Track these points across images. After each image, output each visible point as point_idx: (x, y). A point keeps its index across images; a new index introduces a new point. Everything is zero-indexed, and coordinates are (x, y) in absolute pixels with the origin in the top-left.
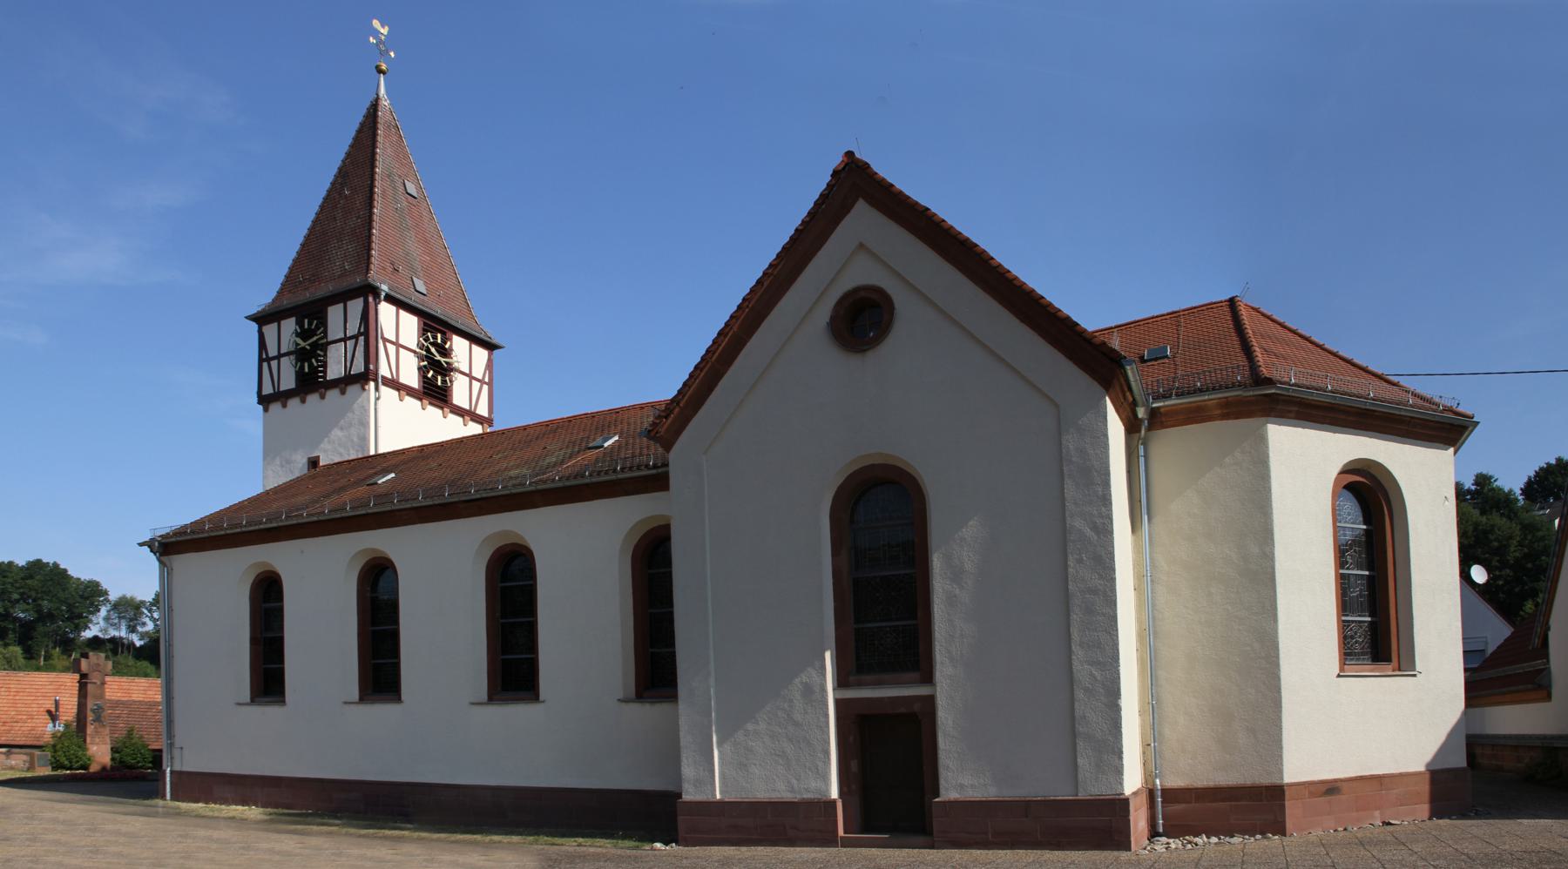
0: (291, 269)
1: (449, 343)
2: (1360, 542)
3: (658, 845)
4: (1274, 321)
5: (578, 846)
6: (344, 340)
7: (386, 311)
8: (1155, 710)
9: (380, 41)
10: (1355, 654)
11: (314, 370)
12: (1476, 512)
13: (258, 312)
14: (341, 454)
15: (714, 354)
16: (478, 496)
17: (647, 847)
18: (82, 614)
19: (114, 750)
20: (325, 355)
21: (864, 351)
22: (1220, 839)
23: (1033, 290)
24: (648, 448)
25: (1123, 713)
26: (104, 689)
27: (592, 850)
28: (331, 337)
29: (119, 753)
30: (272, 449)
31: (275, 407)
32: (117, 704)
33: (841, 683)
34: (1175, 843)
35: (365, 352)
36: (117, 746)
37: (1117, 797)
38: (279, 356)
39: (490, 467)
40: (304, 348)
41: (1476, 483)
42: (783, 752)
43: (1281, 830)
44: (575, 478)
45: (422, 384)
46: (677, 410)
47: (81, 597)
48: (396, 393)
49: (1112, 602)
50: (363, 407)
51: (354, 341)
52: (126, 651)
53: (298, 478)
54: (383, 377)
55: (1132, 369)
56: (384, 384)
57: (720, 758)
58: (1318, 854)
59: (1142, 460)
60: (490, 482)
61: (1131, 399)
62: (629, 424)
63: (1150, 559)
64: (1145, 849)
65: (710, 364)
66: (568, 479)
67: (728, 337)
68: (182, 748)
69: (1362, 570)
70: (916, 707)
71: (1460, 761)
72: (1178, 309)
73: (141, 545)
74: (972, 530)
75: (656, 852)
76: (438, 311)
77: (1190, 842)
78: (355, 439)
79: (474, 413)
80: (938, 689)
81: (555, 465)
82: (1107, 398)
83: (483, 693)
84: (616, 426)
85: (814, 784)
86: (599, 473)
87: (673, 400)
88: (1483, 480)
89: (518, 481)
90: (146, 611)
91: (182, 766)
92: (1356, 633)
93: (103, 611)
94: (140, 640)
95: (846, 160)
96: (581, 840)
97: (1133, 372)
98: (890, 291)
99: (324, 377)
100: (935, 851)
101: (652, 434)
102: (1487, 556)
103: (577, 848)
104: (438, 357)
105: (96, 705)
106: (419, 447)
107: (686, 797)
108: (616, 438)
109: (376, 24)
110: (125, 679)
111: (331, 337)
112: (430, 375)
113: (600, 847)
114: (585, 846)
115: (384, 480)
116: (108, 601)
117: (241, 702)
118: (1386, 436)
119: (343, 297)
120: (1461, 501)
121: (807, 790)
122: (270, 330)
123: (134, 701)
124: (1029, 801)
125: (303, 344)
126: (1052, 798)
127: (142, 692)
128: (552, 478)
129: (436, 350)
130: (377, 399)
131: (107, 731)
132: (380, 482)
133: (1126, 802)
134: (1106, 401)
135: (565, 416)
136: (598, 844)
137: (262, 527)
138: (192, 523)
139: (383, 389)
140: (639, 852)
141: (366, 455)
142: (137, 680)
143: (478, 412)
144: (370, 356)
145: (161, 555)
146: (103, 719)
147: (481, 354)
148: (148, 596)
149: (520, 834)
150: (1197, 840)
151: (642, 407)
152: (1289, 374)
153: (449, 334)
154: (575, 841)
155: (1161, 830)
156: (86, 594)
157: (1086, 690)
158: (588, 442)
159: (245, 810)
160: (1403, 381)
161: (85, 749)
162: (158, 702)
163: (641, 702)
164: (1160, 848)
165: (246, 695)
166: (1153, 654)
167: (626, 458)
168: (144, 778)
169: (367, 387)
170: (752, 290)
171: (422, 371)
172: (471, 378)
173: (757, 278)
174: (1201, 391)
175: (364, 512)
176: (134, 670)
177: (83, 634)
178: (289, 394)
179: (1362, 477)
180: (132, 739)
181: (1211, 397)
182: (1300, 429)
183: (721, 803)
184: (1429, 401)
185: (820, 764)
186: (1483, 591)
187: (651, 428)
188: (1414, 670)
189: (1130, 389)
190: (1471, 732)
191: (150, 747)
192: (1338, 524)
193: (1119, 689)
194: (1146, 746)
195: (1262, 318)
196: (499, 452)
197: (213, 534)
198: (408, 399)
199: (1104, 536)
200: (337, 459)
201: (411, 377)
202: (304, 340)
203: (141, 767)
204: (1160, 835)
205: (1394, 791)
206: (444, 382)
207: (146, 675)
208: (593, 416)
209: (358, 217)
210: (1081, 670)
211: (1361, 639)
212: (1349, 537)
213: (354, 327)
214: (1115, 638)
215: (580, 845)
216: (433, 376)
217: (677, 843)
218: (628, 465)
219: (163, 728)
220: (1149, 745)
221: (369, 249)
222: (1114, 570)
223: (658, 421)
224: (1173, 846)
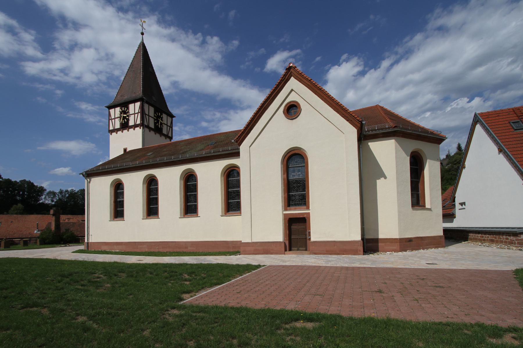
38: (115, 119)
51: (137, 114)
70: (305, 216)
76: (122, 101)
98: (299, 102)
122: (112, 111)
143: (169, 135)
205: (426, 241)
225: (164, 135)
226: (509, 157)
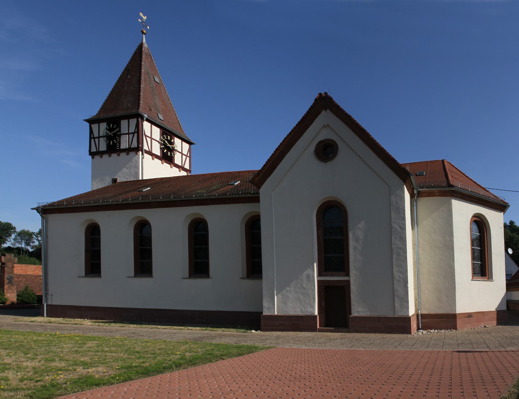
0: (104, 104)
1: (173, 140)
2: (478, 238)
3: (253, 331)
4: (454, 167)
5: (223, 331)
6: (129, 134)
7: (146, 125)
8: (419, 288)
9: (143, 22)
10: (476, 274)
11: (115, 145)
12: (510, 232)
13: (89, 119)
14: (127, 178)
15: (274, 156)
16: (185, 199)
17: (249, 332)
18: (2, 236)
19: (18, 296)
20: (120, 139)
21: (327, 162)
22: (438, 331)
23: (383, 148)
24: (251, 186)
25: (409, 289)
26: (13, 269)
27: (228, 333)
28: (122, 132)
29: (21, 297)
30: (94, 176)
31: (97, 158)
32: (20, 276)
33: (320, 274)
34: (425, 332)
35: (137, 140)
36: (20, 294)
37: (407, 316)
38: (99, 137)
39: (190, 188)
40: (110, 135)
41: (510, 223)
42: (299, 298)
43: (456, 328)
44: (224, 195)
45: (162, 154)
46: (261, 174)
47: (2, 229)
48: (151, 157)
49: (405, 252)
50: (137, 161)
51: (132, 135)
52: (24, 254)
53: (107, 186)
54: (145, 150)
55: (413, 177)
56: (145, 153)
57: (277, 300)
58: (466, 336)
59: (415, 207)
60: (190, 194)
61: (412, 187)
62: (244, 177)
63: (417, 239)
64: (416, 334)
65: (273, 159)
66: (221, 195)
67: (279, 151)
68: (52, 295)
69: (478, 247)
71: (504, 308)
72: (428, 161)
73: (32, 209)
74: (362, 225)
75: (253, 334)
76: (169, 127)
77: (429, 332)
78: (133, 173)
79: (184, 167)
80: (351, 278)
81: (216, 190)
82: (405, 186)
83: (187, 274)
84: (239, 178)
85: (310, 310)
86: (233, 194)
87: (260, 171)
88: (512, 223)
89: (201, 195)
90: (34, 237)
91: (52, 302)
92: (477, 267)
93: (13, 236)
94: (32, 249)
95: (319, 96)
96: (224, 329)
97: (413, 178)
99: (120, 147)
100: (350, 334)
101: (253, 182)
102: (513, 245)
103: (223, 332)
104: (169, 145)
105: (10, 276)
106: (160, 178)
107: (265, 313)
108: (239, 182)
109: (141, 14)
110: (24, 265)
111: (122, 132)
112: (165, 151)
113: (231, 332)
114: (226, 331)
115: (146, 190)
116: (16, 232)
117: (80, 276)
118: (485, 207)
119: (128, 117)
120: (506, 228)
121: (307, 312)
122: (95, 127)
123: (28, 275)
124: (380, 317)
125: (110, 133)
126: (387, 316)
127: (33, 271)
128: (214, 194)
129: (168, 142)
130: (143, 158)
131: (15, 287)
132: (144, 190)
133: (410, 318)
134: (404, 187)
135: (220, 172)
136: (231, 331)
137: (90, 205)
138: (57, 201)
139: (145, 155)
140: (246, 333)
141: (138, 179)
142: (30, 266)
143: (185, 167)
144: (140, 141)
145: (42, 214)
146: (13, 282)
147: (186, 146)
148: (36, 231)
149: (200, 327)
150: (431, 331)
151: (249, 172)
152: (458, 184)
153: (173, 136)
154: (222, 330)
155: (421, 328)
156: (4, 229)
157: (398, 281)
158: (228, 183)
159: (82, 321)
160: (490, 191)
161: (4, 295)
162: (41, 275)
163: (249, 279)
164: (420, 334)
165: (83, 273)
166: (418, 270)
167: (243, 190)
168: (33, 307)
169: (138, 153)
170: (288, 136)
171: (162, 150)
172: (182, 154)
173: (290, 132)
174: (433, 187)
175: (137, 202)
176: (28, 261)
177: (3, 245)
179: (479, 219)
180: (27, 291)
181: (436, 189)
182: (461, 202)
183: (277, 316)
184: (497, 197)
185: (312, 303)
186: (512, 256)
187: (252, 180)
188: (492, 279)
189: (412, 184)
190: (259, 203)
191: (36, 294)
192: (472, 233)
193: (408, 281)
194: (416, 300)
195: (451, 166)
196: (194, 183)
197: (67, 207)
198: (155, 159)
199: (403, 230)
200: (125, 180)
201: (156, 150)
202: (110, 132)
203: (32, 303)
204: (420, 329)
206: (171, 154)
207: (34, 264)
208: (230, 173)
209: (134, 87)
210: (396, 274)
211: (478, 269)
212: (474, 237)
213: (132, 129)
214: (406, 264)
215: (223, 331)
216: (166, 151)
217: (260, 330)
218: (244, 192)
219: (43, 287)
220: (417, 300)
221: (139, 100)
222: (406, 242)
223: (254, 178)
224: (424, 333)
225: (177, 166)
226: (235, 350)
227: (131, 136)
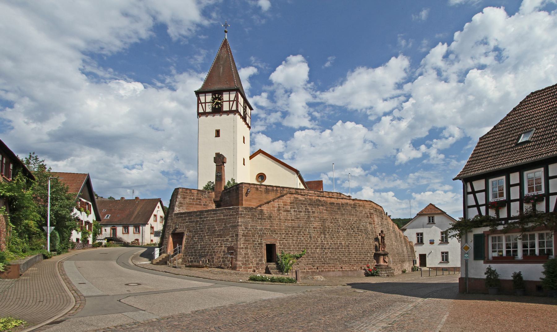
54: (174, 248)
119: (229, 91)
178: (209, 113)
227: (231, 103)
